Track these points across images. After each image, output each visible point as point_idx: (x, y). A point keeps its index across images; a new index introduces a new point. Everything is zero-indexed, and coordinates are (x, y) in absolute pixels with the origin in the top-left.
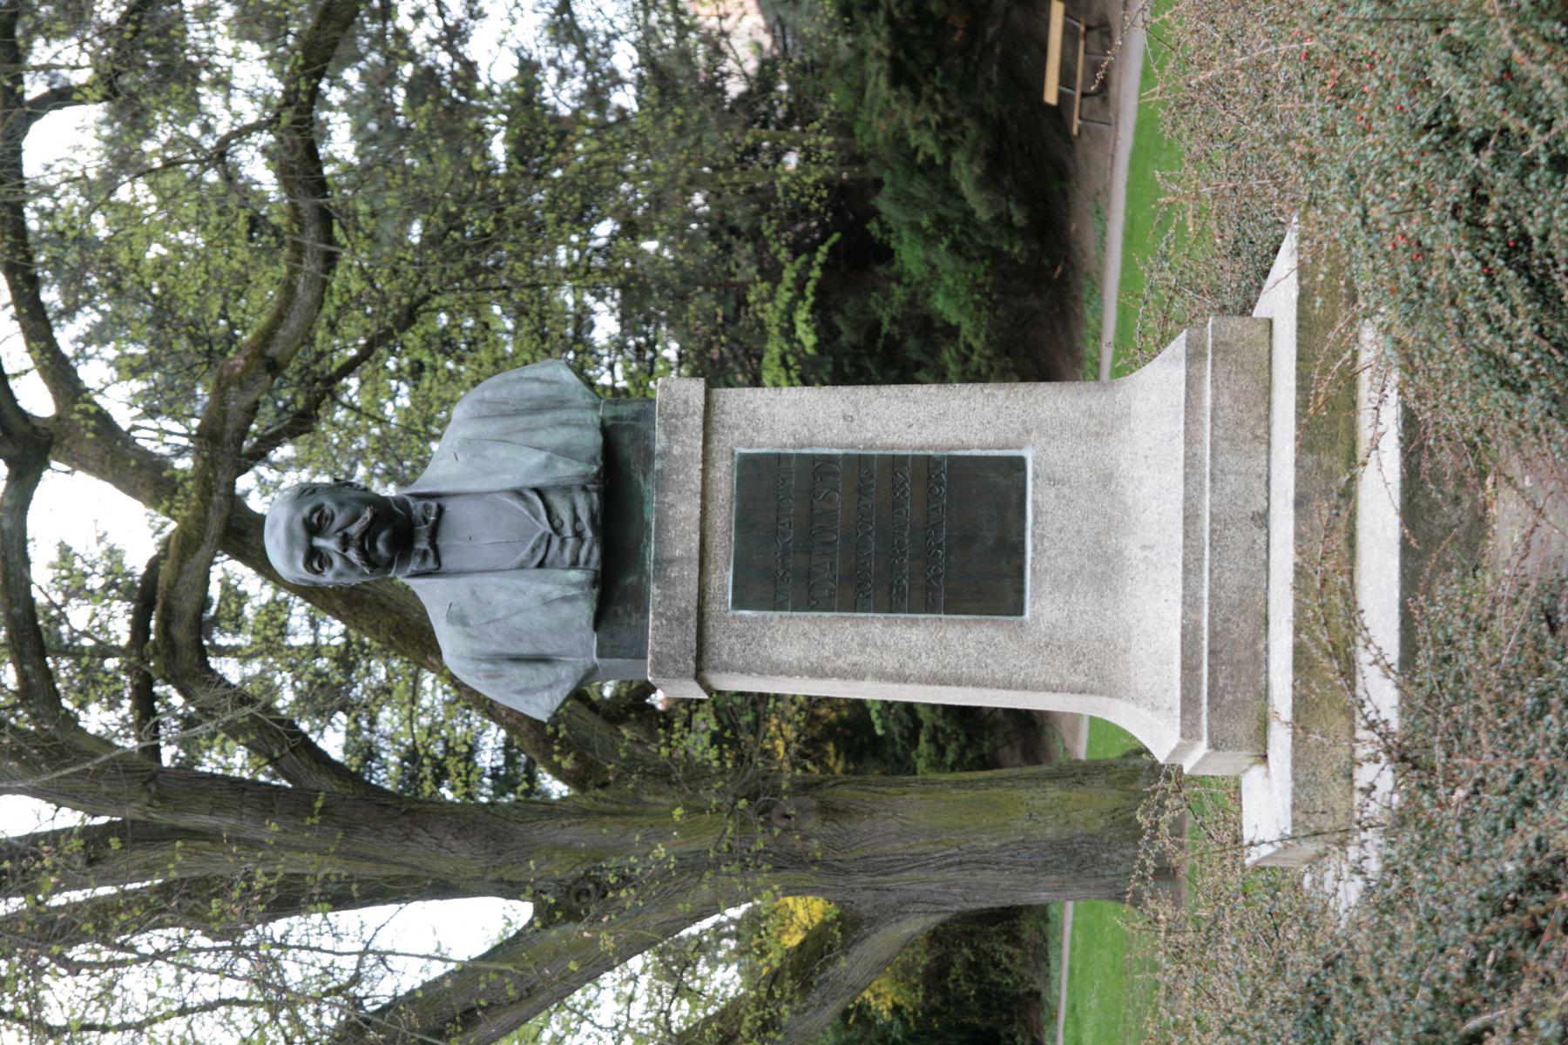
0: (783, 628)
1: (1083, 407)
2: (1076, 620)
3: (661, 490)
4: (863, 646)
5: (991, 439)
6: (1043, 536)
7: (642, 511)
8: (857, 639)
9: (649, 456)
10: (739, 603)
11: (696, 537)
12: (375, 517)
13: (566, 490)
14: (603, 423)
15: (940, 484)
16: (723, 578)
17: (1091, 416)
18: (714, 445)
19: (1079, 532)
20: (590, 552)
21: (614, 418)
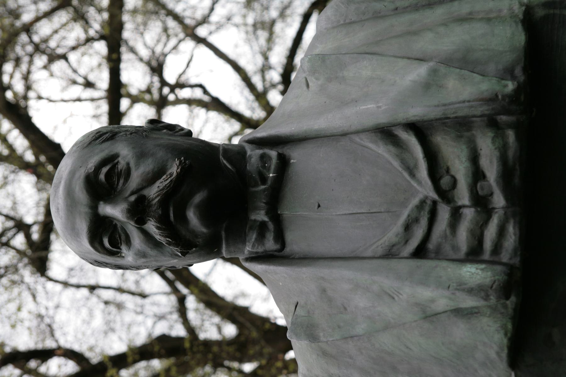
13: (461, 125)
20: (502, 232)
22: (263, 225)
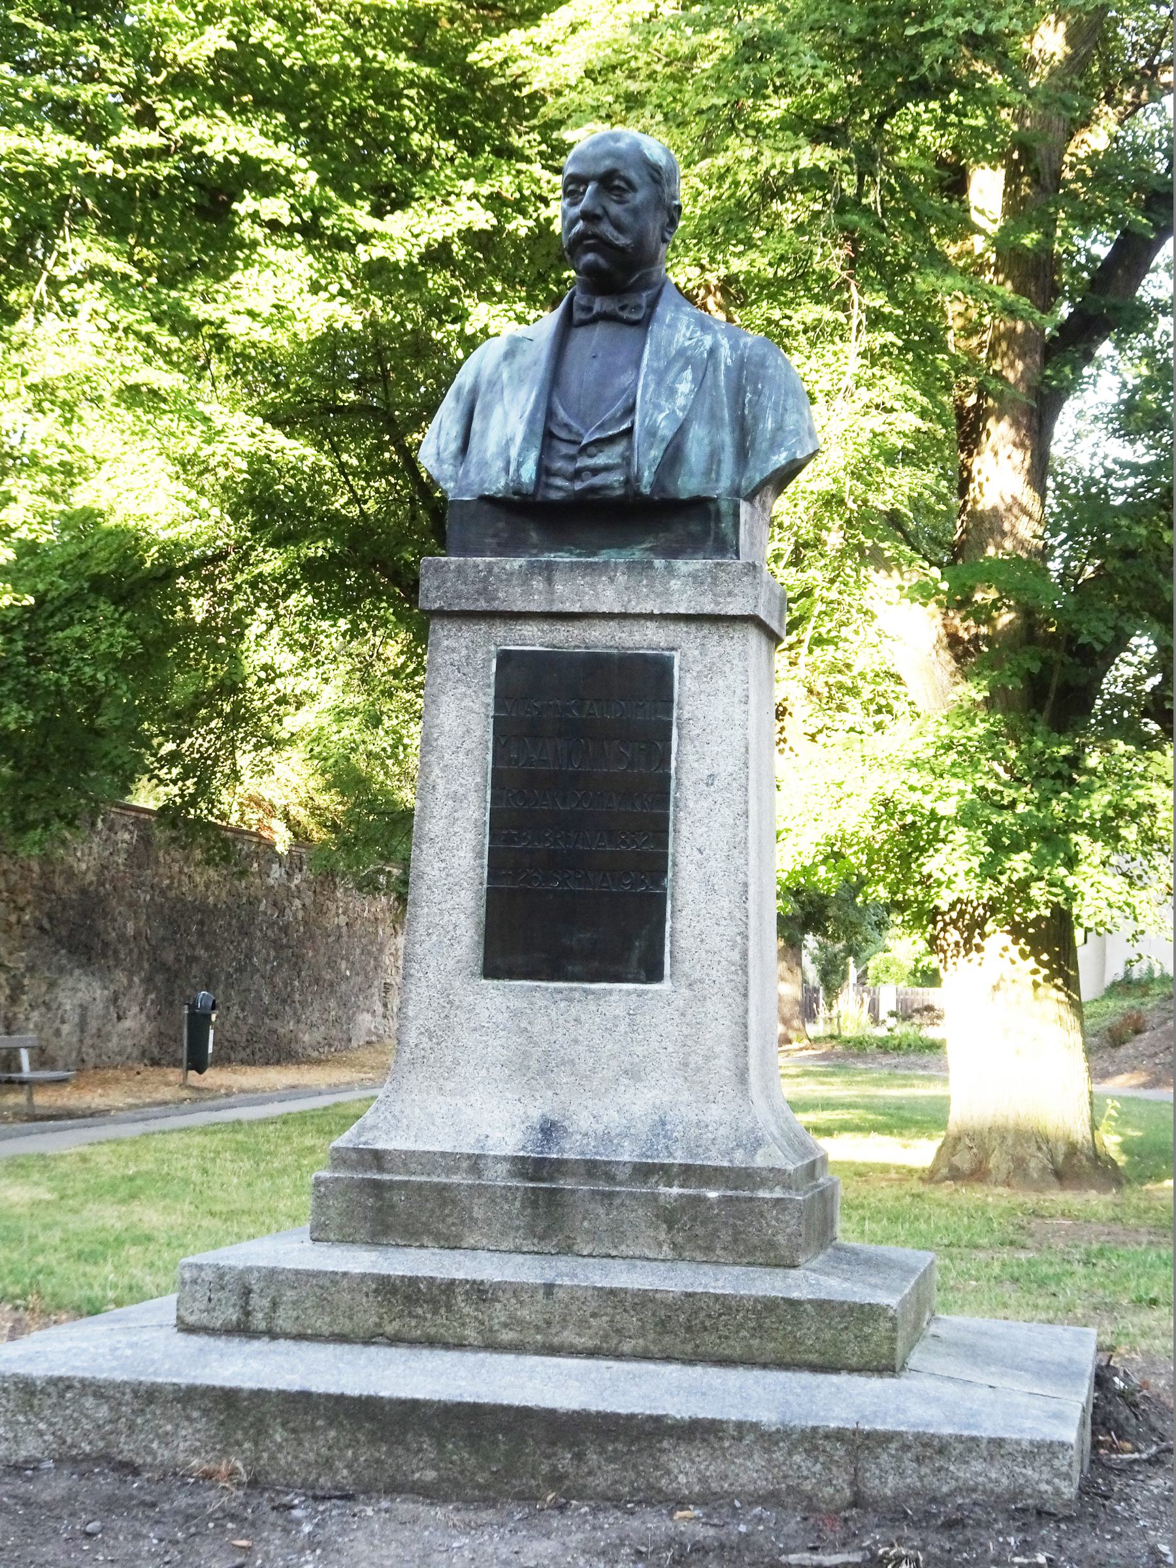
0: (476, 707)
1: (717, 1049)
2: (476, 1035)
3: (631, 567)
4: (455, 797)
5: (683, 943)
6: (570, 1000)
7: (610, 547)
8: (461, 791)
9: (673, 552)
10: (505, 658)
11: (576, 609)
12: (622, 250)
13: (627, 461)
14: (714, 501)
15: (633, 885)
16: (532, 638)
17: (707, 1059)
18: (682, 627)
19: (576, 1041)
20: (559, 488)
21: (718, 512)
22: (590, 309)
